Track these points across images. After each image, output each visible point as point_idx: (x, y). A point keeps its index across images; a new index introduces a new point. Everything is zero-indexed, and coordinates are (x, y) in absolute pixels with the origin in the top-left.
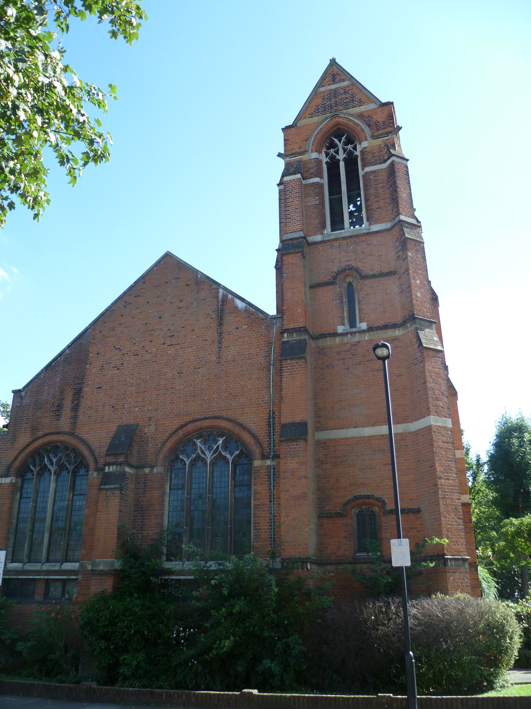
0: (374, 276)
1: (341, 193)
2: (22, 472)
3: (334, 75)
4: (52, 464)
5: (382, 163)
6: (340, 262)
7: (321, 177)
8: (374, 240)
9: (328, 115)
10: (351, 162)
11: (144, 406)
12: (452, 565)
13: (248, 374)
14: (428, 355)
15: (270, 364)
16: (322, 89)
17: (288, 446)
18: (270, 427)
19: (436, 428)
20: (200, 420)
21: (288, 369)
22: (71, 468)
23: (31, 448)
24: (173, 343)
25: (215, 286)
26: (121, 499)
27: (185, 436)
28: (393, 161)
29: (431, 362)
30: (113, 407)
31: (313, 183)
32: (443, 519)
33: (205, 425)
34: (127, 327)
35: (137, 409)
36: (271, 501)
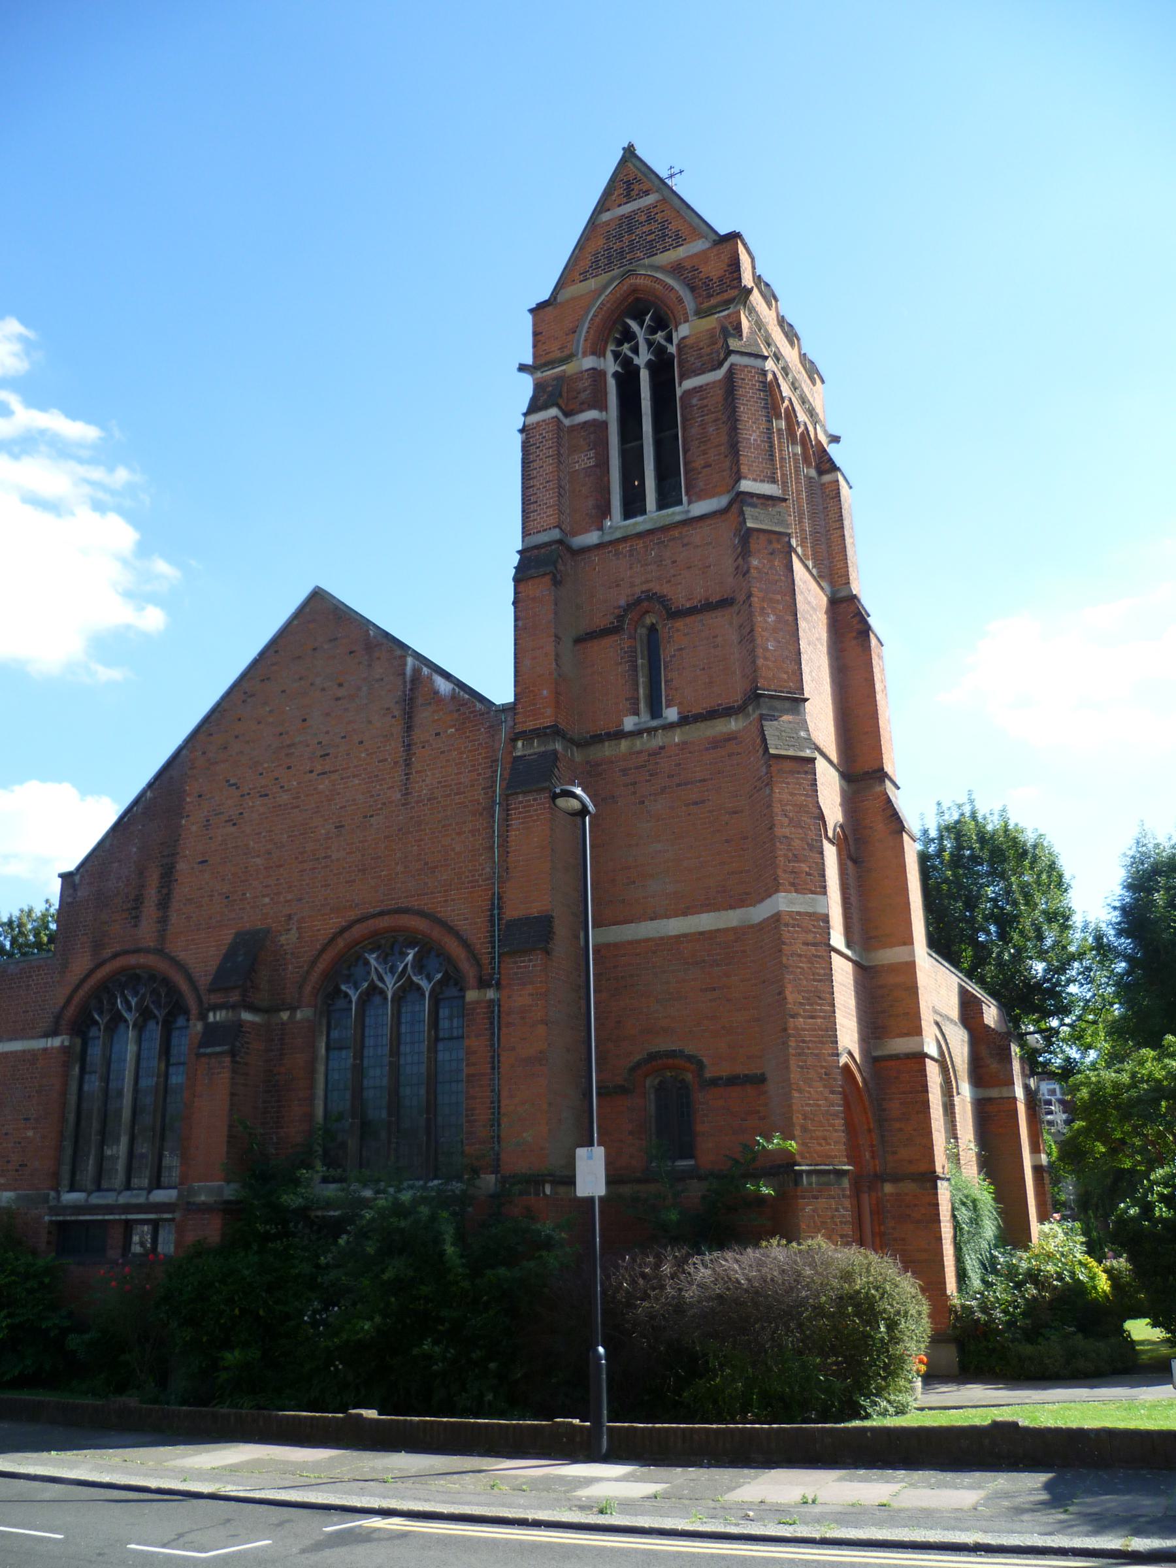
2: (81, 1027)
3: (629, 184)
5: (714, 370)
6: (632, 585)
7: (603, 407)
8: (696, 535)
9: (616, 272)
10: (662, 368)
11: (279, 894)
12: (810, 1184)
13: (457, 824)
15: (494, 802)
16: (606, 217)
17: (516, 962)
18: (493, 926)
19: (791, 917)
20: (374, 916)
21: (520, 813)
22: (160, 1014)
23: (92, 982)
24: (327, 768)
25: (399, 652)
26: (234, 1071)
28: (732, 365)
29: (788, 783)
30: (227, 897)
31: (585, 423)
32: (796, 1095)
33: (386, 925)
34: (248, 742)
35: (267, 900)
36: (493, 1068)
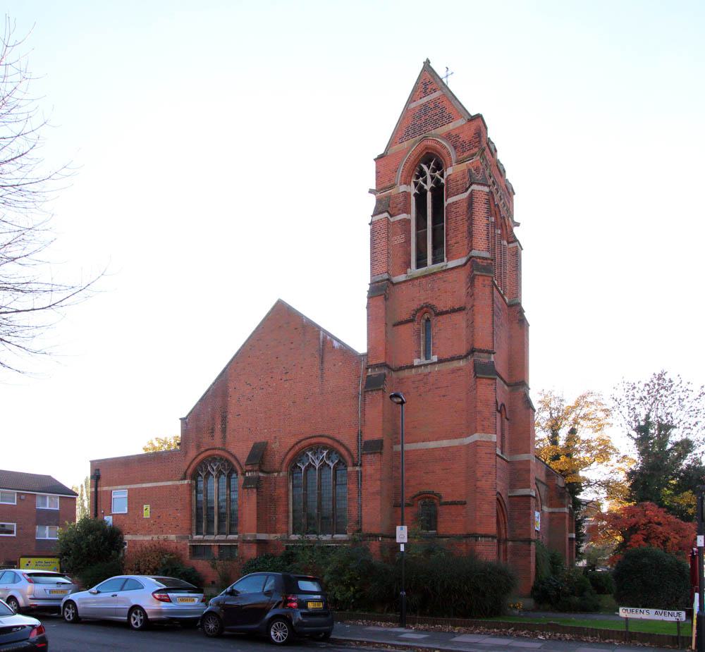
0: (447, 312)
1: (426, 228)
2: (195, 476)
4: (214, 470)
6: (420, 300)
8: (448, 275)
10: (438, 191)
14: (481, 384)
22: (226, 473)
25: (317, 329)
26: (257, 494)
27: (300, 449)
31: (400, 220)
35: (266, 431)
